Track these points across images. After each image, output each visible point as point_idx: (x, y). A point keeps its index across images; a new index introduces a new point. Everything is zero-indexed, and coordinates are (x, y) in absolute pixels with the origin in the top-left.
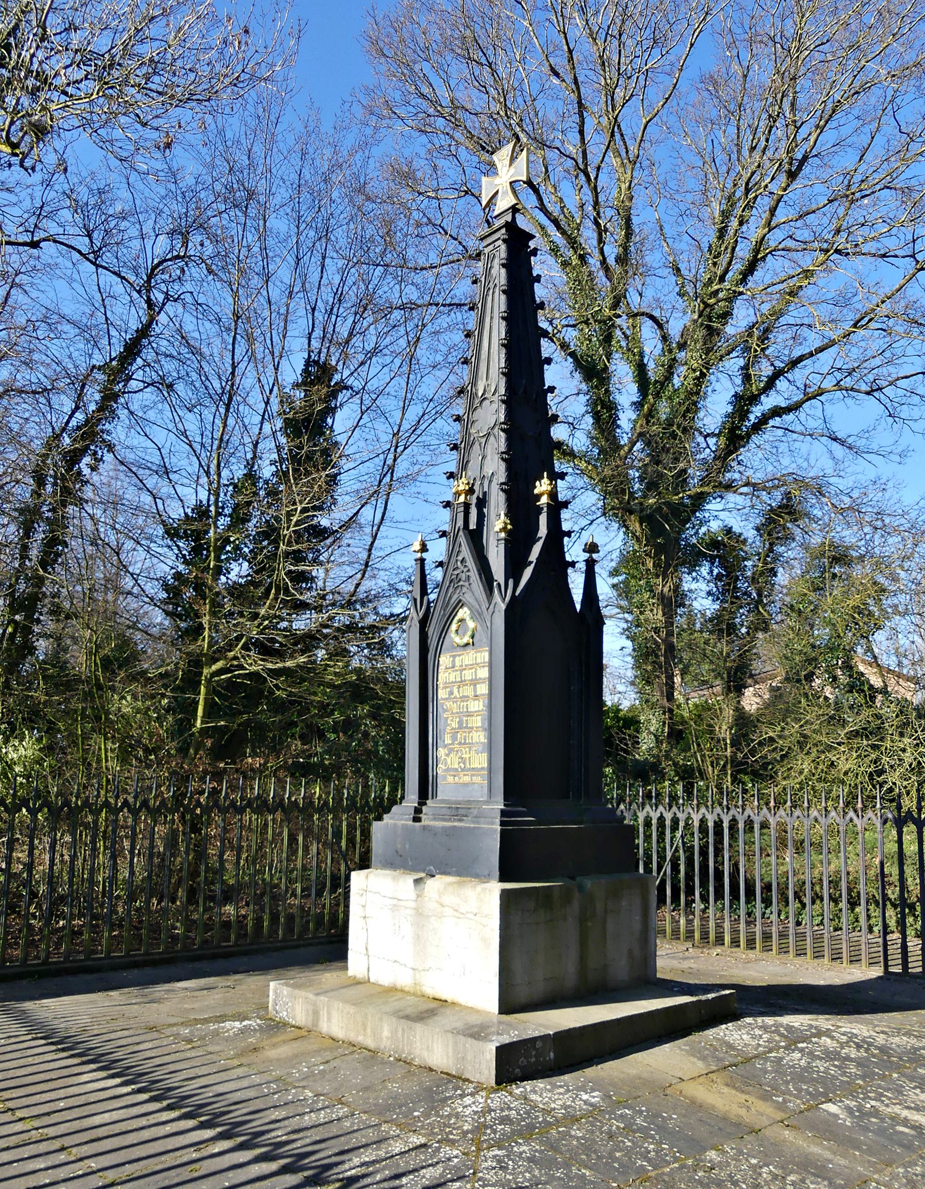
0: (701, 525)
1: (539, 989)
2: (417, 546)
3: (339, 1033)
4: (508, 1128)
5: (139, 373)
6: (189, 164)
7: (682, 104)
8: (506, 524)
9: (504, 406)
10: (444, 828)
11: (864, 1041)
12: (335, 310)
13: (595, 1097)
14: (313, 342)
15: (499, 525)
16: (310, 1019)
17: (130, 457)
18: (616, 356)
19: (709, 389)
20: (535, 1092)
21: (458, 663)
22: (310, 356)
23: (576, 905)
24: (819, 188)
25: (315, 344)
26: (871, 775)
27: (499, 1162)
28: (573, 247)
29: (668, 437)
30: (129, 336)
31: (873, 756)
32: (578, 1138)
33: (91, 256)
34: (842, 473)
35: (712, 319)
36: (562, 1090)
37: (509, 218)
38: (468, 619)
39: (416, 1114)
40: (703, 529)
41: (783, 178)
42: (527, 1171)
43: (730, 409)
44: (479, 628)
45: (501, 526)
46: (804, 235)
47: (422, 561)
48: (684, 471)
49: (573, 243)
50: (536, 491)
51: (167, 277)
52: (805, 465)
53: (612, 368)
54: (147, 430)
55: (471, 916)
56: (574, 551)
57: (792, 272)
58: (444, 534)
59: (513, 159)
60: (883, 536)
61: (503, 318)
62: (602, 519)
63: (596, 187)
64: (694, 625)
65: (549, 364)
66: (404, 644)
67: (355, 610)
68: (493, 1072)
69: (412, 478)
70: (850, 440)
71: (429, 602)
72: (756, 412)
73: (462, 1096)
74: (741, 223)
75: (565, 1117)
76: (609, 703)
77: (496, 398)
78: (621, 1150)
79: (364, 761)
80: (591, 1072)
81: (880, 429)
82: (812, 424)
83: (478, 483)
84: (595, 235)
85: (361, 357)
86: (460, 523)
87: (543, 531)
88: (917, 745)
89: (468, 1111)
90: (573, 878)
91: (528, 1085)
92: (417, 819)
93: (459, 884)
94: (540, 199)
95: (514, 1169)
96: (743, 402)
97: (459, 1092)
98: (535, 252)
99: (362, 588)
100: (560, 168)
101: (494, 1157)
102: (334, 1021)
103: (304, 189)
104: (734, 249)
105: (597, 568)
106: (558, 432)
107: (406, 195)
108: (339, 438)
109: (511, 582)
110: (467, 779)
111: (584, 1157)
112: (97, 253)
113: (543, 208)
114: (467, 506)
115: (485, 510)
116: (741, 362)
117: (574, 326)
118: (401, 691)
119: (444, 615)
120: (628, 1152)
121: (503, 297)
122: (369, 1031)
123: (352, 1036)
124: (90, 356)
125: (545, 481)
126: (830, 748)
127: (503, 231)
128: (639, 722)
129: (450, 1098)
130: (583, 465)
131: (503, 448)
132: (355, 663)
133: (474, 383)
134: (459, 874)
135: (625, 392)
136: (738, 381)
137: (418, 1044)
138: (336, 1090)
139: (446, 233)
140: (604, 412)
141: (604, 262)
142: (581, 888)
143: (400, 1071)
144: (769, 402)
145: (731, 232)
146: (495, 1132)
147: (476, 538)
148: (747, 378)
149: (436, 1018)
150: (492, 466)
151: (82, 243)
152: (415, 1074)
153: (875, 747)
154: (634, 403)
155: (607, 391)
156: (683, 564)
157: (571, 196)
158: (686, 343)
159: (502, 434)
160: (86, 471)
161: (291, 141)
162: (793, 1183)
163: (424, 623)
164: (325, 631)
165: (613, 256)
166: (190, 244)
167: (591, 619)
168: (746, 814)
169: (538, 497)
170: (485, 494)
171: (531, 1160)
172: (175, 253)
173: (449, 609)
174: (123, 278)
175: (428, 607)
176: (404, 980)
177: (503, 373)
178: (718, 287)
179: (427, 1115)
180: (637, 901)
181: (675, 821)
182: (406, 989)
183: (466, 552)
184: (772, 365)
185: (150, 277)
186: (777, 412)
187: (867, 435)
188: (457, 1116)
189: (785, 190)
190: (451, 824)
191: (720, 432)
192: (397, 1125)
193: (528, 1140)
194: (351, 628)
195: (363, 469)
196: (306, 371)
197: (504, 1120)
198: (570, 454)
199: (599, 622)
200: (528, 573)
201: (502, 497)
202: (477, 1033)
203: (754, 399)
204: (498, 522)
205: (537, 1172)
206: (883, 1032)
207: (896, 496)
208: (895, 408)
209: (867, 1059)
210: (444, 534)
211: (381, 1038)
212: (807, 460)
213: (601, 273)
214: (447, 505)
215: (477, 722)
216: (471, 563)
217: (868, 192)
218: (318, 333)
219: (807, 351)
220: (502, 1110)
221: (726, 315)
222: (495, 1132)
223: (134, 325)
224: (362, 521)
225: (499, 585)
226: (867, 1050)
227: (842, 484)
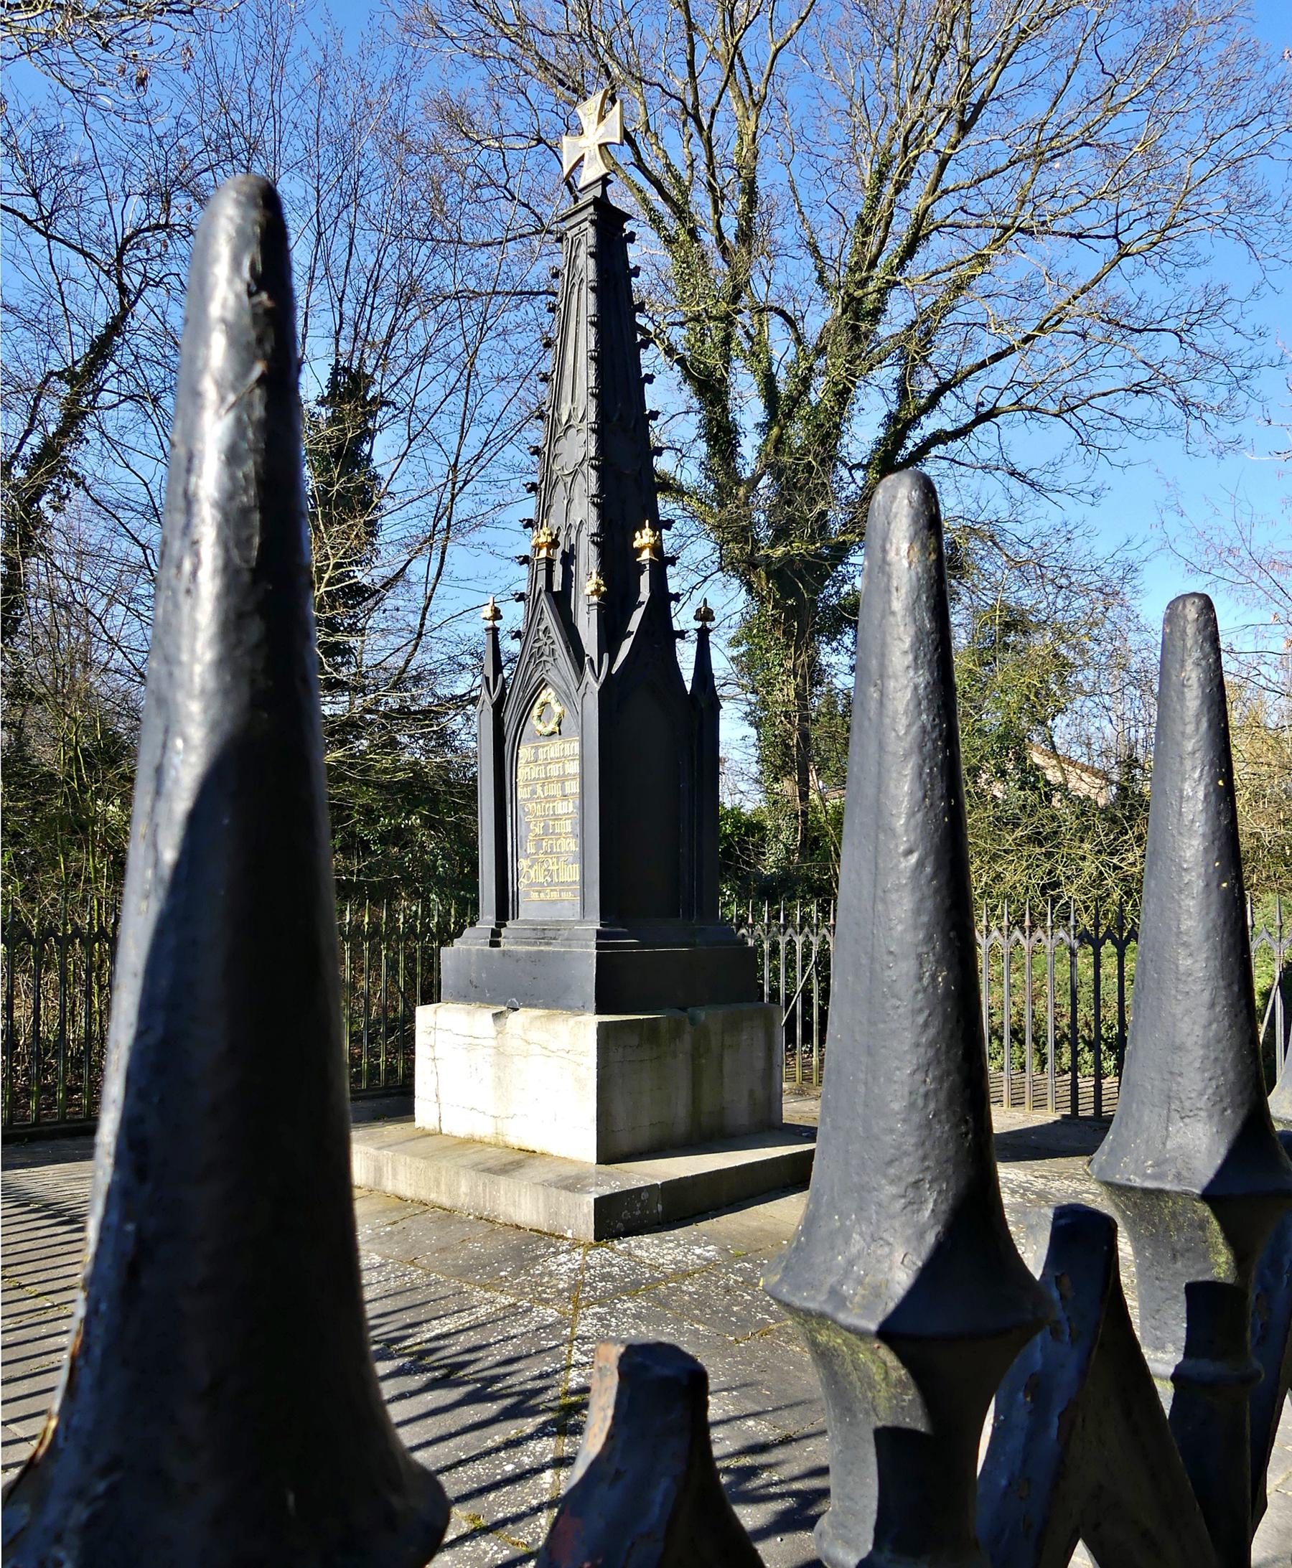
0: (844, 582)
1: (644, 1136)
2: (487, 612)
3: (407, 1191)
4: (610, 1286)
5: (112, 386)
6: (169, 97)
7: (823, 23)
8: (597, 584)
9: (594, 436)
10: (528, 953)
11: (1020, 1186)
12: (369, 301)
13: (711, 1252)
14: (342, 342)
15: (590, 586)
16: (372, 1175)
17: (109, 494)
18: (737, 364)
19: (855, 407)
20: (640, 1247)
21: (541, 757)
22: (337, 362)
23: (687, 1038)
24: (998, 145)
25: (345, 347)
26: (1044, 888)
27: (600, 1319)
28: (679, 218)
29: (803, 469)
30: (95, 333)
31: (1048, 866)
32: (690, 1294)
33: (40, 224)
34: (1020, 518)
35: (859, 315)
36: (671, 1245)
37: (597, 192)
38: (553, 702)
39: (502, 1274)
40: (846, 588)
41: (952, 129)
42: (632, 1327)
43: (881, 433)
44: (567, 713)
45: (593, 587)
46: (977, 206)
47: (495, 631)
48: (823, 514)
49: (681, 212)
50: (636, 544)
51: (142, 253)
52: (974, 507)
53: (731, 379)
54: (126, 457)
55: (563, 1054)
56: (683, 618)
57: (961, 258)
58: (521, 597)
59: (602, 117)
60: (1067, 597)
61: (592, 323)
62: (720, 574)
63: (709, 140)
64: (835, 707)
65: (651, 382)
66: (472, 733)
67: (406, 691)
68: (592, 1227)
69: (475, 523)
70: (1031, 475)
71: (504, 681)
72: (915, 438)
73: (556, 1254)
74: (897, 191)
75: (675, 1273)
76: (728, 806)
77: (584, 426)
78: (739, 1304)
79: (419, 881)
80: (704, 1226)
81: (1068, 461)
82: (985, 454)
83: (563, 533)
84: (710, 202)
85: (404, 362)
86: (542, 583)
87: (645, 594)
88: (1099, 852)
89: (563, 1269)
90: (684, 1009)
91: (633, 1241)
92: (495, 944)
93: (548, 1017)
94: (637, 153)
95: (617, 1326)
96: (898, 426)
97: (552, 1249)
98: (631, 237)
99: (413, 664)
100: (663, 116)
101: (595, 1314)
102: (401, 1177)
103: (324, 139)
104: (888, 224)
105: (712, 637)
106: (664, 464)
107: (456, 145)
108: (379, 471)
109: (606, 656)
110: (555, 895)
111: (697, 1312)
112: (48, 219)
113: (640, 165)
114: (550, 562)
115: (573, 568)
116: (897, 372)
117: (682, 324)
118: (471, 793)
119: (523, 697)
120: (747, 1306)
121: (592, 296)
122: (443, 1187)
123: (423, 1195)
124: (46, 360)
125: (647, 531)
126: (995, 858)
127: (591, 209)
128: (764, 828)
129: (542, 1256)
130: (695, 504)
131: (593, 491)
132: (406, 757)
133: (556, 406)
134: (547, 1007)
135: (749, 411)
136: (893, 396)
137: (503, 1199)
138: (407, 1252)
139: (514, 198)
140: (721, 436)
141: (721, 238)
142: (693, 1021)
143: (482, 1229)
144: (931, 424)
145: (884, 201)
146: (595, 1289)
147: (562, 602)
148: (903, 394)
149: (522, 1171)
150: (580, 511)
151: (27, 205)
152: (499, 1233)
153: (1049, 855)
154: (757, 425)
155: (725, 409)
156: (819, 632)
157: (676, 147)
158: (825, 348)
159: (593, 472)
160: (49, 513)
161: (306, 74)
163: (498, 707)
164: (368, 716)
165: (733, 231)
166: (173, 210)
167: (705, 700)
169: (639, 551)
170: (572, 547)
171: (635, 1316)
172: (153, 222)
173: (530, 690)
174: (86, 255)
175: (503, 689)
176: (482, 1129)
177: (593, 395)
178: (916, 152)
179: (515, 1275)
180: (760, 1035)
181: (807, 945)
182: (486, 1140)
183: (549, 620)
184: (936, 376)
185: (121, 251)
186: (940, 438)
187: (1052, 469)
188: (551, 1274)
189: (954, 147)
190: (536, 948)
191: (869, 463)
192: (481, 1286)
193: (632, 1297)
194: (403, 712)
195: (411, 510)
196: (333, 383)
197: (604, 1278)
198: (678, 491)
199: (715, 706)
200: (626, 646)
202: (572, 1184)
203: (912, 423)
204: (588, 583)
205: (643, 1329)
206: (1042, 1177)
207: (1087, 547)
208: (1088, 435)
209: (1022, 1205)
210: (521, 597)
211: (459, 1196)
212: (977, 500)
213: (717, 254)
214: (526, 560)
215: (567, 826)
216: (555, 633)
217: (1062, 150)
218: (348, 331)
219: (980, 360)
220: (603, 1267)
221: (876, 314)
222: (595, 1289)
223: (102, 319)
224: (414, 579)
225: (591, 660)
226: (1023, 1195)
227: (1023, 531)
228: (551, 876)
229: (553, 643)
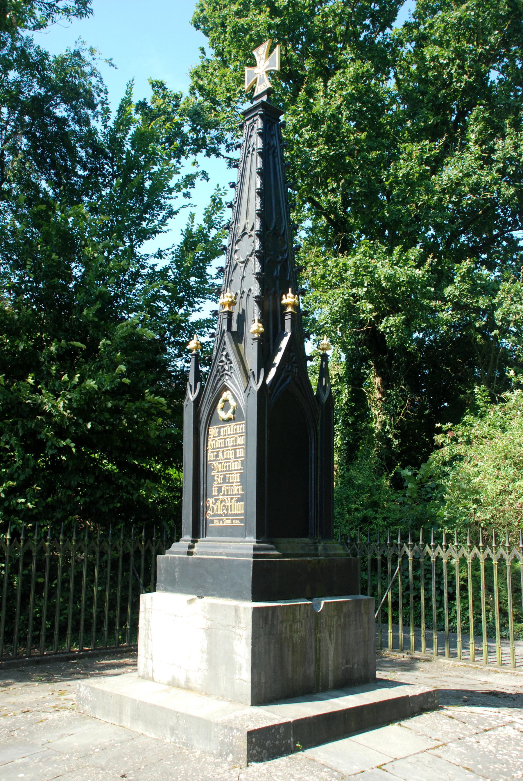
59: (271, 51)
86: (225, 327)
168: (512, 554)
170: (243, 311)
173: (216, 393)
201: (256, 309)
229: (231, 363)
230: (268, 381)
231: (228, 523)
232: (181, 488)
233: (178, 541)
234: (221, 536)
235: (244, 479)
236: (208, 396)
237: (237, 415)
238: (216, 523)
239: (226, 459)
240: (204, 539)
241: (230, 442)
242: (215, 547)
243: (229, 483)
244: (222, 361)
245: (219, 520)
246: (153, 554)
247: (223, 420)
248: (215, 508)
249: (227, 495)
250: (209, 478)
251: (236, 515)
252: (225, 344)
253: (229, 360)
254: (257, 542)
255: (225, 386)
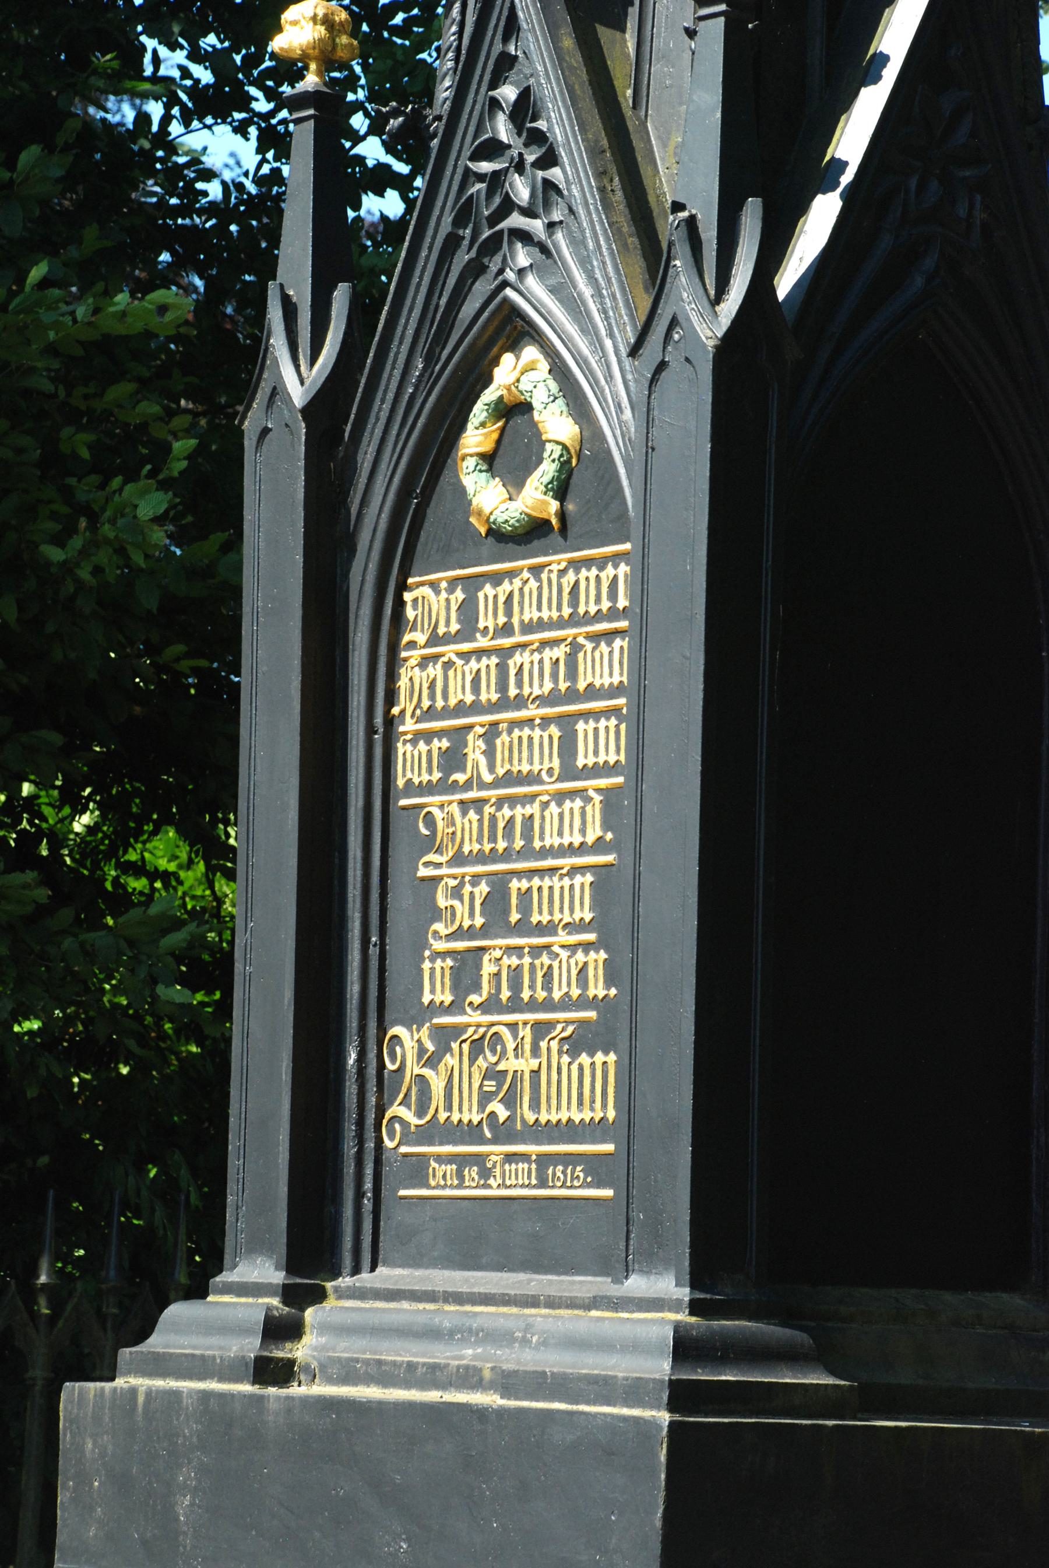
162: (4, 839)
173: (453, 353)
228: (510, 1101)
229: (549, 159)
230: (785, 284)
231: (514, 1183)
232: (228, 958)
233: (198, 1291)
234: (470, 1262)
235: (618, 902)
236: (403, 368)
237: (584, 505)
238: (442, 1184)
239: (510, 779)
240: (365, 1279)
241: (536, 670)
242: (432, 1334)
243: (523, 928)
244: (492, 149)
245: (462, 1161)
246: (38, 1373)
247: (495, 533)
248: (437, 1084)
249: (515, 1005)
250: (401, 900)
251: (570, 1131)
252: (512, 28)
253: (537, 138)
254: (695, 1307)
255: (514, 312)
